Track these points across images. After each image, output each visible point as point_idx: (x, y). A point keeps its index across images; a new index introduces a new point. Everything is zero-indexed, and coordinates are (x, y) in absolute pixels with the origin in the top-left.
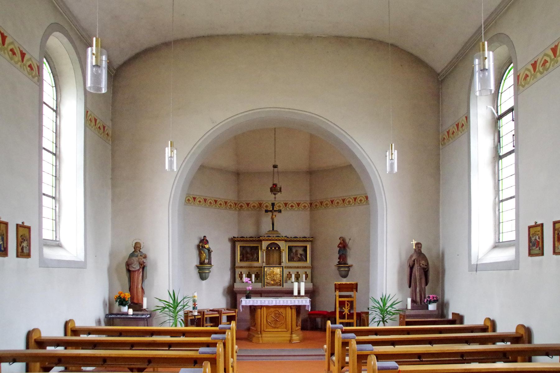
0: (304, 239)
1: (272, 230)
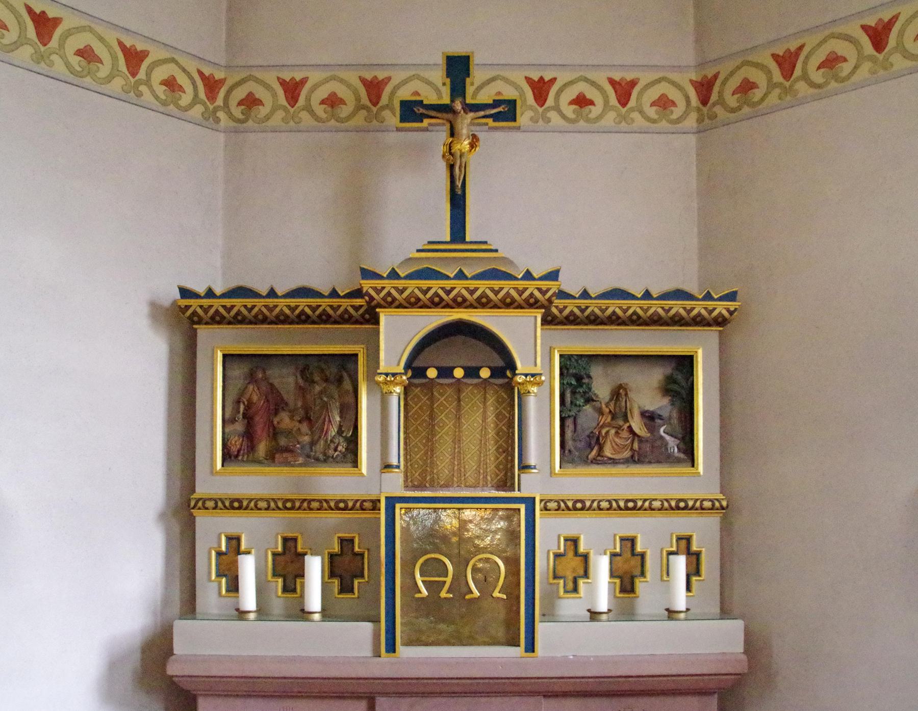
0: (677, 307)
1: (448, 239)
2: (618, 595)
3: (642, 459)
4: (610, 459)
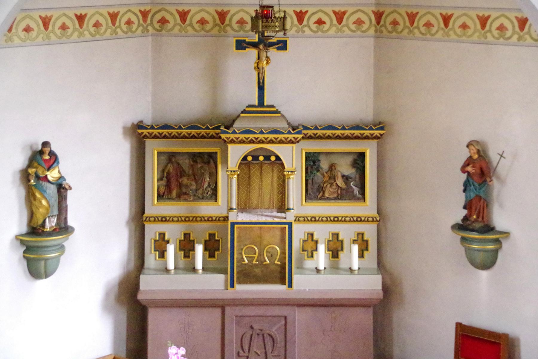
1: (257, 104)
2: (331, 259)
3: (342, 198)
4: (328, 198)
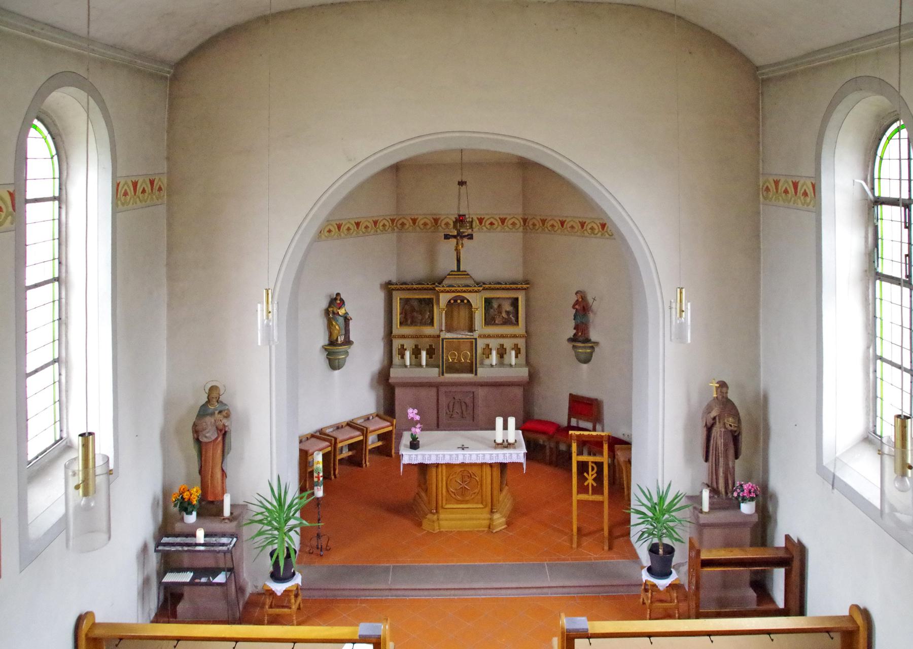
1: (456, 270)
